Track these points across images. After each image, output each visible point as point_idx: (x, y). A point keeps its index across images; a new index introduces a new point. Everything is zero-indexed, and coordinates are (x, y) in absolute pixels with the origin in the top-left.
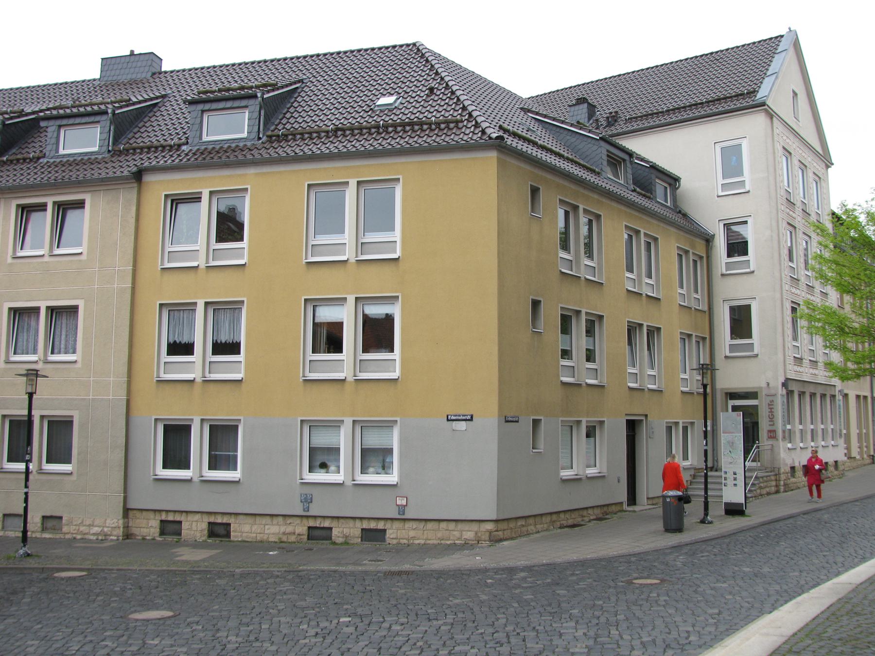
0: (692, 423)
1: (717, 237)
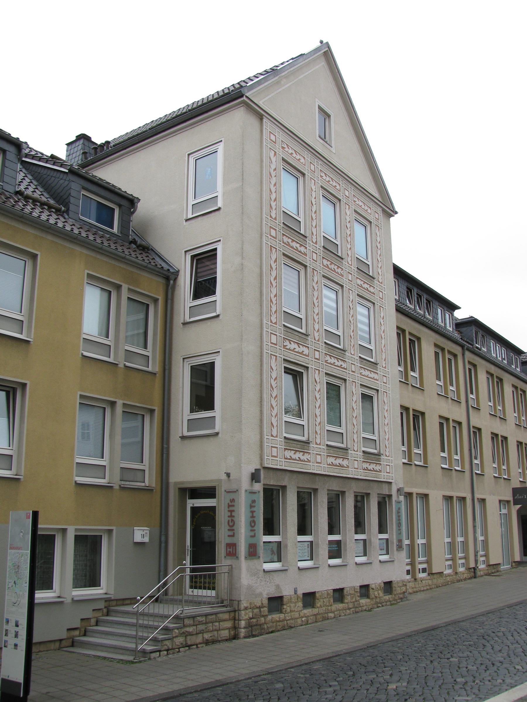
0: (110, 531)
1: (181, 273)
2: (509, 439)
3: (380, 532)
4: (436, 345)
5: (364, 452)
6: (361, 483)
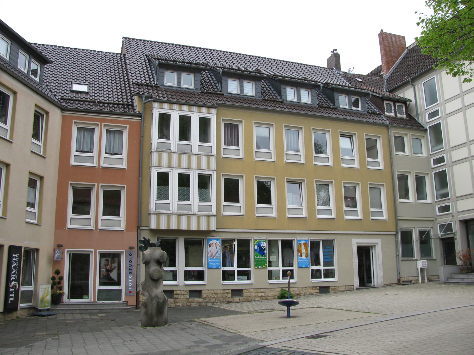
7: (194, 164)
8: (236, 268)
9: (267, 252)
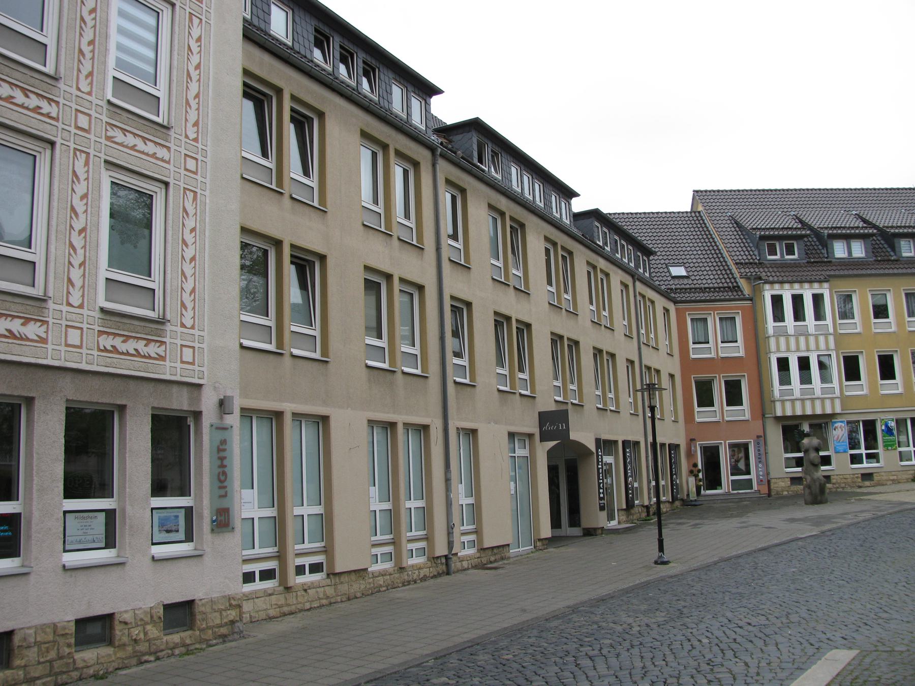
2: (533, 327)
3: (159, 489)
4: (547, 239)
5: (102, 310)
6: (96, 382)
7: (812, 345)
8: (863, 451)
9: (895, 432)
